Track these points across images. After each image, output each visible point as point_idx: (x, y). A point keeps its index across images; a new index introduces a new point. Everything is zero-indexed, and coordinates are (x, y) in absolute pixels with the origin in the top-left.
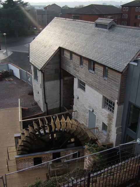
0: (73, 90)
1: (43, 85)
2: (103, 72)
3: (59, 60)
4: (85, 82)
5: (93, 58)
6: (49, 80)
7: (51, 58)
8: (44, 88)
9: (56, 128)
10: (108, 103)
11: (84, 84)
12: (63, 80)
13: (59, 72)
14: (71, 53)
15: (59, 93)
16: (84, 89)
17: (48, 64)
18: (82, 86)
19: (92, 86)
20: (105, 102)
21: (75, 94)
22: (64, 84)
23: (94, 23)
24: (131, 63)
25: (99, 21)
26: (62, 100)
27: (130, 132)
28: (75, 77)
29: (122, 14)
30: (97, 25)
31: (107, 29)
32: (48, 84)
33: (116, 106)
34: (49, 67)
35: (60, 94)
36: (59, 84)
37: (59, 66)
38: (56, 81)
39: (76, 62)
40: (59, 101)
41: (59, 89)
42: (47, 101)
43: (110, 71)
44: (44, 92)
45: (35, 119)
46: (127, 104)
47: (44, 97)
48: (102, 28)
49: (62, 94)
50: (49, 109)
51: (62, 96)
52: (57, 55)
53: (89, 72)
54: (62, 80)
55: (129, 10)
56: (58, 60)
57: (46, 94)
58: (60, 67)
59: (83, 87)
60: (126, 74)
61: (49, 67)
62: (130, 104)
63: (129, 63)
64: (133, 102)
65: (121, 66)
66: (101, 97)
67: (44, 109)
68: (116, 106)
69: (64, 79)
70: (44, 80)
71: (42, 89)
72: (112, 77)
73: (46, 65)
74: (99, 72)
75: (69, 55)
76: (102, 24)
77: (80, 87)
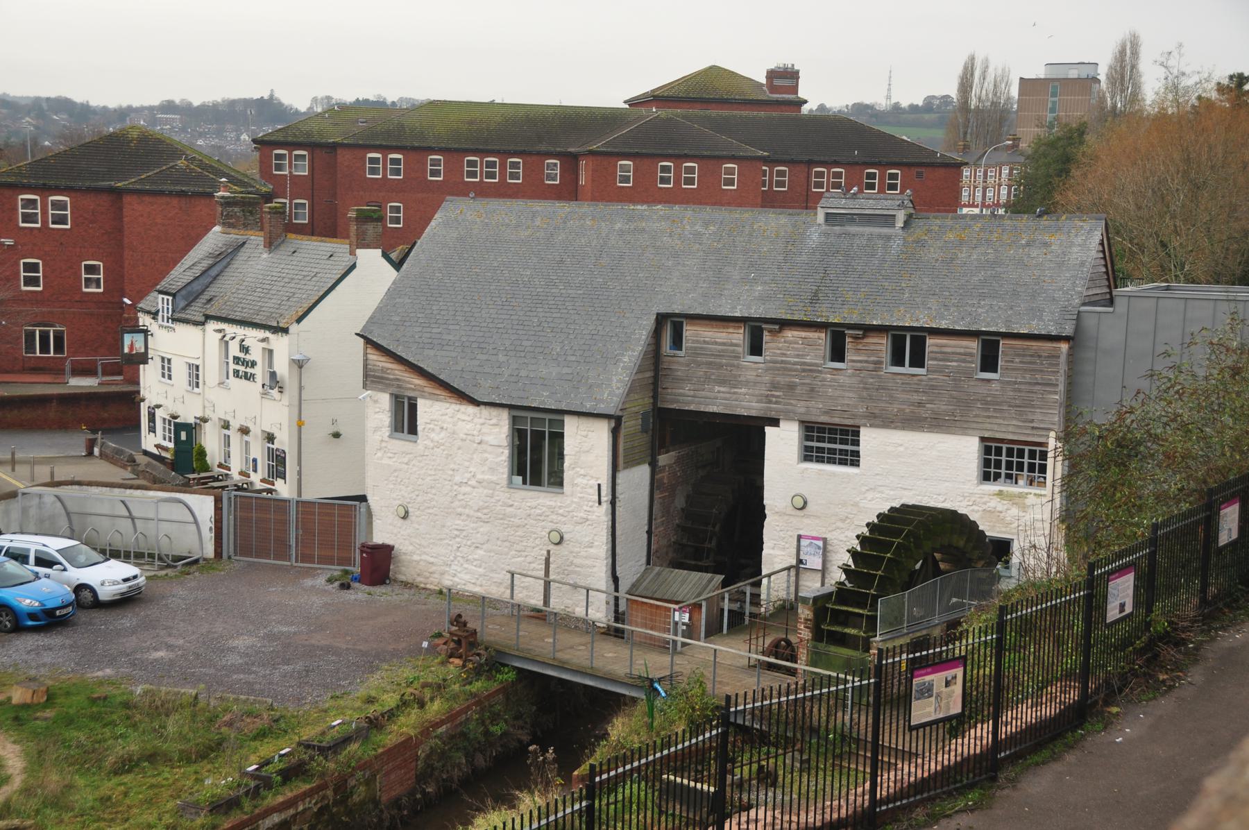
8: (613, 503)
11: (851, 435)
15: (646, 528)
16: (852, 459)
28: (775, 422)
35: (649, 533)
39: (798, 356)
58: (655, 404)
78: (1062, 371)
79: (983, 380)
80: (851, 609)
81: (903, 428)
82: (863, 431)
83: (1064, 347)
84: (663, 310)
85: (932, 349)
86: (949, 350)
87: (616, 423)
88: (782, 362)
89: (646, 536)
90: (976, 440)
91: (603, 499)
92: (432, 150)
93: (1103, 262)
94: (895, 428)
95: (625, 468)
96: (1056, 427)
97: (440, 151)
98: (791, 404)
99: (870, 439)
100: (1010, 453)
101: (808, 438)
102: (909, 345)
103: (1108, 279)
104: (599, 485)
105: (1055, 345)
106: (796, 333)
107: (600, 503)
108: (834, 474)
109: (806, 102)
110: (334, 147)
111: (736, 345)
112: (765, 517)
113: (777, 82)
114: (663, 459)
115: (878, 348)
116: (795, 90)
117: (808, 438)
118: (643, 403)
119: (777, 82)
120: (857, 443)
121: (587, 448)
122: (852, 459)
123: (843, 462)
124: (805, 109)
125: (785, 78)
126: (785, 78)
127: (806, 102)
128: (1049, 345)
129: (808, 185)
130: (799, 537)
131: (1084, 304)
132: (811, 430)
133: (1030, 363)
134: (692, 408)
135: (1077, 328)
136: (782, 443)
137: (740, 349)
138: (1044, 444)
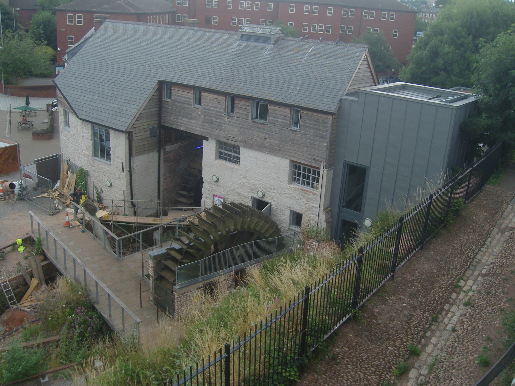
1: (128, 165)
2: (289, 119)
3: (158, 109)
5: (257, 95)
8: (130, 171)
10: (302, 174)
11: (236, 149)
12: (164, 152)
13: (158, 134)
14: (198, 91)
15: (157, 180)
16: (236, 161)
19: (260, 147)
22: (166, 160)
27: (350, 215)
28: (207, 139)
29: (174, 13)
32: (138, 161)
33: (324, 175)
35: (159, 182)
37: (158, 122)
39: (214, 107)
43: (302, 113)
44: (129, 181)
46: (340, 167)
48: (257, 42)
49: (161, 184)
52: (155, 97)
54: (162, 151)
55: (189, 4)
57: (133, 185)
58: (160, 123)
63: (341, 99)
64: (353, 160)
68: (324, 175)
69: (165, 149)
71: (126, 175)
72: (310, 124)
73: (135, 119)
74: (280, 119)
77: (220, 158)
78: (329, 131)
79: (293, 130)
81: (257, 150)
83: (330, 118)
84: (164, 79)
85: (136, 138)
86: (278, 113)
87: (129, 135)
88: (208, 109)
89: (157, 184)
90: (288, 162)
91: (124, 170)
94: (254, 149)
96: (324, 160)
98: (211, 131)
99: (244, 153)
100: (304, 170)
101: (221, 148)
102: (262, 108)
103: (373, 79)
104: (123, 163)
105: (326, 116)
106: (213, 96)
107: (123, 171)
111: (189, 99)
112: (203, 183)
114: (168, 148)
115: (247, 107)
117: (221, 148)
118: (153, 122)
120: (239, 153)
121: (118, 145)
122: (236, 161)
128: (323, 116)
130: (214, 196)
131: (347, 95)
132: (221, 144)
133: (314, 124)
134: (174, 127)
135: (340, 108)
136: (209, 150)
137: (192, 101)
138: (319, 168)
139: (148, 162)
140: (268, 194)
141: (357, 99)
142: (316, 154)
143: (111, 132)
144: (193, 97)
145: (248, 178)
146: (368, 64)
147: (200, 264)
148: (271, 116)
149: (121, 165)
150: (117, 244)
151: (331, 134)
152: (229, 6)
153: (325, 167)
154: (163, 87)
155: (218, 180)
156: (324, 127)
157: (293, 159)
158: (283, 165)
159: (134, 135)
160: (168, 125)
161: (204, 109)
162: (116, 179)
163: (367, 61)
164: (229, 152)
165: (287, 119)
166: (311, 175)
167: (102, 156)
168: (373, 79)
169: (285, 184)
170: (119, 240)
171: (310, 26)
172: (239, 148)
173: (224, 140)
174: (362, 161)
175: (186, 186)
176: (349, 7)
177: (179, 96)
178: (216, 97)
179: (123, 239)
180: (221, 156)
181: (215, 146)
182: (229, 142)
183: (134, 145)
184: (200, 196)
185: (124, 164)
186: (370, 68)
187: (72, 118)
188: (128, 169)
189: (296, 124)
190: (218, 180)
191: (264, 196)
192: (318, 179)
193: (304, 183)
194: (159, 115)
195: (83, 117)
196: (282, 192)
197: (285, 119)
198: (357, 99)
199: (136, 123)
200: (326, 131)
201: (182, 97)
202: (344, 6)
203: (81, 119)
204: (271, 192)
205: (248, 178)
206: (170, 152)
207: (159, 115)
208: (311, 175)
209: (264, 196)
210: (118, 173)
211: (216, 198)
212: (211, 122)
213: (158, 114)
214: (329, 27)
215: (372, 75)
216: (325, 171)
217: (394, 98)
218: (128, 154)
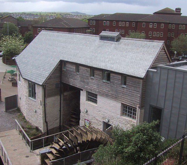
0: (79, 104)
2: (120, 81)
4: (97, 94)
6: (50, 96)
7: (52, 72)
8: (45, 105)
9: (78, 141)
11: (95, 96)
13: (60, 86)
15: (59, 110)
16: (95, 101)
17: (49, 78)
18: (92, 97)
19: (106, 95)
20: (124, 109)
21: (82, 108)
22: (64, 100)
23: (99, 36)
24: (149, 70)
25: (103, 33)
26: (62, 118)
28: (82, 90)
30: (103, 38)
31: (114, 41)
32: (49, 100)
33: (138, 111)
34: (51, 82)
35: (60, 111)
36: (60, 99)
38: (56, 97)
39: (85, 74)
40: (59, 119)
41: (59, 106)
42: (47, 120)
45: (45, 138)
46: (148, 107)
47: (44, 115)
49: (62, 111)
50: (49, 129)
51: (62, 114)
53: (102, 82)
56: (58, 74)
57: (46, 112)
58: (61, 81)
59: (95, 100)
60: (147, 79)
61: (51, 82)
62: (151, 106)
64: (154, 104)
65: (142, 75)
66: (119, 105)
67: (44, 129)
68: (138, 111)
70: (45, 96)
72: (131, 84)
75: (75, 68)
76: (112, 37)
80: (36, 140)
82: (98, 96)
83: (141, 81)
88: (82, 75)
91: (42, 104)
92: (114, 21)
93: (165, 54)
95: (48, 97)
97: (115, 21)
99: (99, 99)
103: (169, 59)
108: (93, 106)
109: (182, 14)
110: (98, 20)
113: (177, 10)
114: (65, 94)
116: (180, 12)
119: (177, 10)
121: (39, 92)
122: (95, 101)
123: (93, 102)
124: (182, 15)
125: (178, 10)
126: (178, 10)
127: (182, 14)
129: (178, 28)
131: (151, 68)
138: (136, 108)
139: (54, 101)
140: (111, 121)
141: (156, 70)
142: (135, 100)
143: (36, 85)
144: (76, 68)
145: (101, 112)
146: (165, 51)
147: (64, 160)
148: (112, 79)
149: (40, 102)
150: (30, 143)
151: (142, 89)
152: (162, 27)
153: (139, 107)
154: (62, 63)
155: (87, 111)
156: (138, 86)
157: (123, 103)
158: (118, 106)
159: (46, 87)
160: (65, 82)
161: (81, 75)
162: (34, 111)
163: (165, 49)
164: (92, 97)
165: (120, 81)
166: (132, 111)
167: (33, 96)
168: (169, 59)
169: (119, 116)
170: (31, 142)
171: (152, 33)
172: (97, 95)
173: (90, 91)
174: (161, 105)
175: (72, 114)
176: (172, 24)
177: (69, 68)
178: (86, 68)
179: (33, 141)
180: (89, 99)
181: (86, 94)
182: (92, 92)
183: (47, 92)
184: (78, 119)
185: (42, 101)
186: (166, 53)
187: (21, 78)
188: (44, 104)
189: (125, 84)
190: (87, 111)
191: (109, 121)
192: (136, 114)
193: (128, 115)
194: (61, 77)
195: (24, 77)
196: (118, 120)
197: (118, 81)
198: (156, 70)
199: (48, 81)
200: (140, 88)
201: (71, 68)
202: (169, 23)
203: (23, 78)
204: (112, 119)
205: (101, 112)
206: (66, 95)
207: (61, 77)
208: (132, 111)
209: (109, 121)
210: (39, 105)
211: (86, 121)
212: (84, 82)
213: (60, 77)
214: (162, 34)
215: (168, 57)
216: (139, 110)
217: (177, 71)
218: (44, 97)
